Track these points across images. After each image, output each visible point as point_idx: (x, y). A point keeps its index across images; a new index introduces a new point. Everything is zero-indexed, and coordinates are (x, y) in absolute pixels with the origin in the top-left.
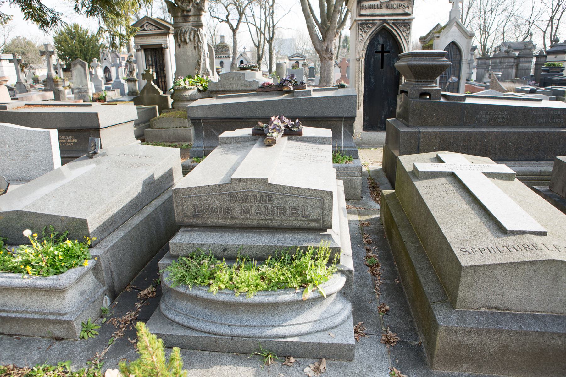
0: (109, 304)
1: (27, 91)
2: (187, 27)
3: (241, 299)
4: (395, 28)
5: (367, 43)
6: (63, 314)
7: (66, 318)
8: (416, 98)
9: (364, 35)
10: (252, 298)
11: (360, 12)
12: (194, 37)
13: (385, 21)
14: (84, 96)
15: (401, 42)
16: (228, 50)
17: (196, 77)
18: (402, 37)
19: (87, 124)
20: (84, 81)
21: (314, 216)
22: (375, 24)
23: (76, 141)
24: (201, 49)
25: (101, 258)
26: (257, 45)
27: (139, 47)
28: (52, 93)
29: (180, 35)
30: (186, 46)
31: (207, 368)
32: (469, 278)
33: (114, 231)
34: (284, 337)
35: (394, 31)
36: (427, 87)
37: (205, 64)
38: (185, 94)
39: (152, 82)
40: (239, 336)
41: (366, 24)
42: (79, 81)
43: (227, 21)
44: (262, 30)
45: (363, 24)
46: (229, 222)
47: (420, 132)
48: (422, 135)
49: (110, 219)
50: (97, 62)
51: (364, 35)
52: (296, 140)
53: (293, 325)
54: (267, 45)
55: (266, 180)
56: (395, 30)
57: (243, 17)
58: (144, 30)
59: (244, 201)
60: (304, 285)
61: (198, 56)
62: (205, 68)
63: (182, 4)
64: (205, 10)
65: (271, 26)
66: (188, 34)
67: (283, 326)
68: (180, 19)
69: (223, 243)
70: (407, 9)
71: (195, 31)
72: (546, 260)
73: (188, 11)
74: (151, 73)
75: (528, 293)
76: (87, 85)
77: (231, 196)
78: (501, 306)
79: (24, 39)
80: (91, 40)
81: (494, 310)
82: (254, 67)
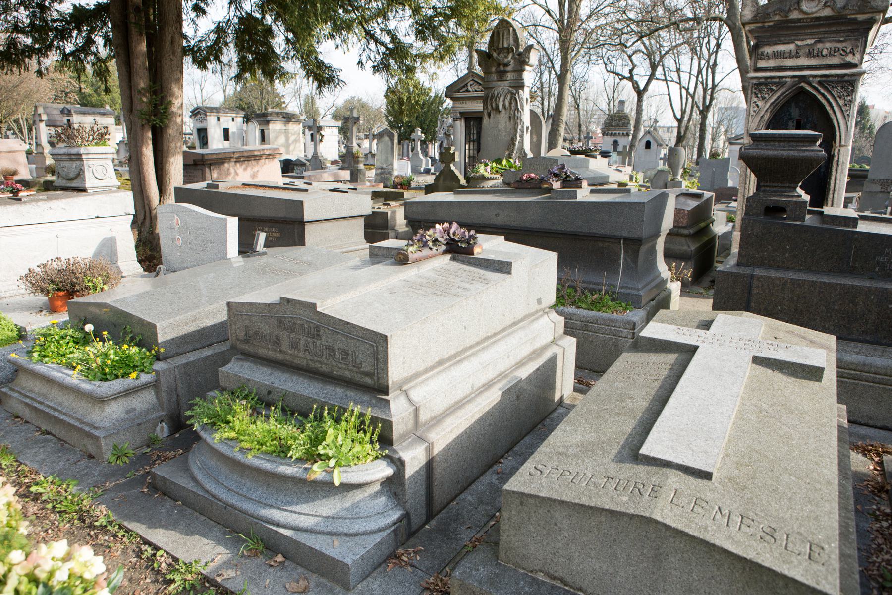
0: (166, 435)
1: (322, 168)
2: (502, 87)
3: (240, 457)
4: (822, 91)
6: (96, 428)
7: (97, 433)
8: (757, 215)
10: (250, 459)
11: (756, 64)
12: (510, 103)
13: (803, 79)
14: (387, 179)
15: (833, 116)
16: (629, 123)
17: (504, 162)
18: (836, 108)
19: (291, 215)
20: (390, 159)
21: (366, 368)
23: (278, 235)
24: (519, 121)
25: (161, 374)
26: (679, 117)
28: (349, 172)
29: (491, 99)
31: (187, 535)
32: (513, 512)
33: (204, 347)
34: (278, 525)
35: (819, 97)
36: (781, 196)
37: (522, 142)
39: (452, 165)
40: (232, 506)
41: (766, 85)
42: (384, 157)
43: (631, 78)
44: (691, 91)
46: (279, 357)
47: (752, 276)
48: (755, 282)
49: (198, 331)
50: (419, 133)
51: (759, 103)
52: (463, 262)
53: (296, 513)
54: (696, 116)
56: (823, 95)
57: (659, 70)
58: (468, 91)
59: (293, 331)
60: (312, 457)
61: (512, 131)
62: (522, 149)
64: (531, 63)
65: (710, 86)
66: (502, 98)
67: (283, 510)
68: (494, 77)
70: (850, 55)
71: (512, 93)
72: (638, 516)
73: (506, 65)
74: (452, 152)
75: (611, 570)
77: (280, 321)
78: (569, 579)
79: (359, 100)
80: (432, 103)
81: (558, 584)
82: (592, 151)
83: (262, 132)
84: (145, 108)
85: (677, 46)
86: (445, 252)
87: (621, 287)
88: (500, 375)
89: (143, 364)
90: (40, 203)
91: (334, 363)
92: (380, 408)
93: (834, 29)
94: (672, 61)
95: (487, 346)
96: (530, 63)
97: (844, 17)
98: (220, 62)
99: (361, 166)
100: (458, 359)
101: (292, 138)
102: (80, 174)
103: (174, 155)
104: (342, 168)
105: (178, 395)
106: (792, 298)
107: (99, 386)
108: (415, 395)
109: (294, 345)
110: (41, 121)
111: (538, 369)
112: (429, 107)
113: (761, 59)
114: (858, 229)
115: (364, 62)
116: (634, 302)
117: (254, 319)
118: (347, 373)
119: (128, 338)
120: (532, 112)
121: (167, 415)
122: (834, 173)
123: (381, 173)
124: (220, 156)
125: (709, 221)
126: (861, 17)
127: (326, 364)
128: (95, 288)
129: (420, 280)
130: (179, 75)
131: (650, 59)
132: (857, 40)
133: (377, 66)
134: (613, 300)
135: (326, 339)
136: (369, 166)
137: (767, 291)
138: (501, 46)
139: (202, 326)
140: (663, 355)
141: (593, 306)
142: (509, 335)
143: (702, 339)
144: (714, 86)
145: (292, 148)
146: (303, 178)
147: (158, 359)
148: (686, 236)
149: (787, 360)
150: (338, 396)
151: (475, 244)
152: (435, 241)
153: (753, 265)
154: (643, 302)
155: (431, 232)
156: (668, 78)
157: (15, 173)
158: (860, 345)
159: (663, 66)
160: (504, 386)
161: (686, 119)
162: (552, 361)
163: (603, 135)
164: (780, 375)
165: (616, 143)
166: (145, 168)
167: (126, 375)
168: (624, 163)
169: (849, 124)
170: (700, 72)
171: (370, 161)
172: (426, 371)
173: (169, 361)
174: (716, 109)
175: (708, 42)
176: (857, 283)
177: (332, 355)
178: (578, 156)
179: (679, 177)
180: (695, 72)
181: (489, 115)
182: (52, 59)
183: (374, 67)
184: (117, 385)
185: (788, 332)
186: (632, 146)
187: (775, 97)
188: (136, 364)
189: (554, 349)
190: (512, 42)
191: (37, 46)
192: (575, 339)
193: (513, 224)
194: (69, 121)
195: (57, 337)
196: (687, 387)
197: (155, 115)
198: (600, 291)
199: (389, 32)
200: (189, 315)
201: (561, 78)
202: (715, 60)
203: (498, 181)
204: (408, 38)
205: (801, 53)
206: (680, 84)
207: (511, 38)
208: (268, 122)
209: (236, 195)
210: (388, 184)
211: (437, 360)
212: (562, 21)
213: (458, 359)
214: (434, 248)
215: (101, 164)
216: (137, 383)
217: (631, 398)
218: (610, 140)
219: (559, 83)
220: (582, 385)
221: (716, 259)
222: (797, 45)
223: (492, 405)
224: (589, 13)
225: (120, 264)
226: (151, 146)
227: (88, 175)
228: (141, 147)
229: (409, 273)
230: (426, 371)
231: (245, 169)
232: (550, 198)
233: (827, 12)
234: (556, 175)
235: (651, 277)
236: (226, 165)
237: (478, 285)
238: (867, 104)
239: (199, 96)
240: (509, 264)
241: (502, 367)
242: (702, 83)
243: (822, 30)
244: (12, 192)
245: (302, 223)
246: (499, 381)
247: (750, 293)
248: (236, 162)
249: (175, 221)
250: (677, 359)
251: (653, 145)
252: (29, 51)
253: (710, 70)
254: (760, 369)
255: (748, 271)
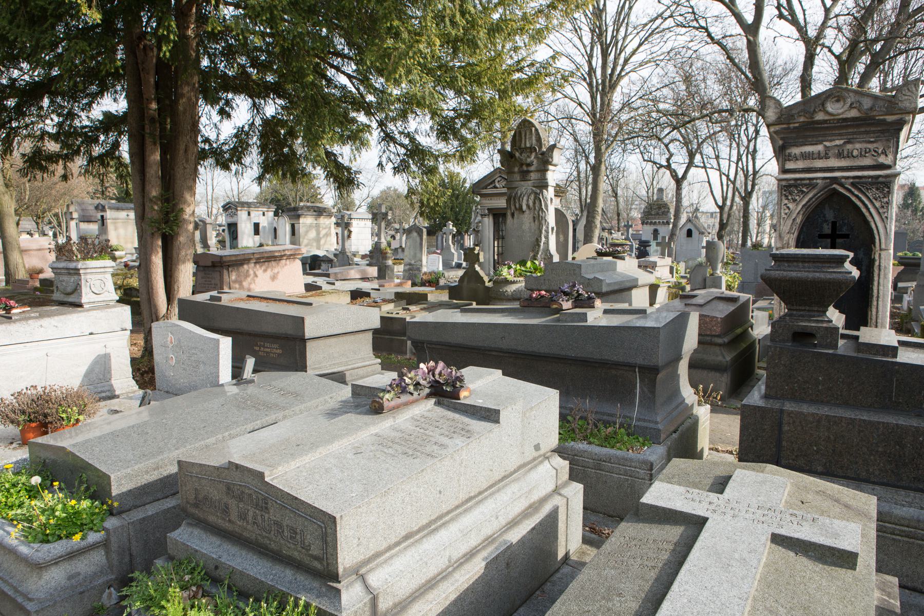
1: (350, 264)
2: (525, 187)
4: (856, 193)
5: (799, 220)
6: (30, 600)
9: (791, 206)
11: (783, 165)
12: (534, 203)
13: (835, 180)
14: (415, 276)
15: (870, 219)
16: (668, 212)
17: (529, 264)
19: (289, 330)
20: (418, 255)
21: (315, 551)
22: (814, 186)
23: (279, 351)
24: (543, 222)
25: (112, 533)
27: (487, 211)
30: (522, 216)
33: (166, 497)
35: (854, 199)
36: (810, 321)
37: (547, 243)
38: (505, 289)
39: (476, 266)
41: (796, 186)
43: (668, 167)
44: (732, 177)
45: (790, 186)
47: (782, 411)
48: (786, 419)
49: (161, 480)
50: (451, 227)
51: (791, 206)
55: (261, 475)
56: (857, 196)
57: (698, 157)
58: (495, 187)
59: (241, 500)
61: (537, 232)
62: (547, 250)
63: (521, 154)
65: (751, 172)
66: (525, 198)
68: (517, 177)
69: (214, 556)
70: (883, 156)
71: (536, 193)
73: (529, 165)
74: (476, 252)
76: (421, 261)
77: (229, 488)
79: (395, 190)
80: (467, 194)
83: (293, 226)
84: (155, 215)
85: (715, 133)
86: (429, 396)
87: (638, 420)
88: (486, 539)
89: (92, 521)
90: (30, 322)
91: (282, 542)
92: (330, 599)
93: (863, 130)
94: (711, 148)
95: (471, 508)
96: (554, 162)
97: (873, 118)
98: (242, 164)
99: (390, 262)
100: (433, 527)
101: (323, 232)
102: (77, 289)
103: (184, 262)
104: (370, 265)
105: (131, 555)
106: (829, 438)
107: (37, 551)
108: (374, 580)
109: (243, 516)
110: (72, 219)
111: (533, 529)
112: (464, 198)
113: (789, 160)
114: (899, 360)
115: (384, 164)
116: (652, 437)
117: (204, 482)
118: (296, 553)
119: (82, 488)
120: (557, 210)
121: (116, 579)
122: (876, 278)
123: (410, 269)
124: (239, 258)
125: (746, 326)
126: (890, 118)
127: (275, 542)
128: (69, 419)
129: (394, 434)
130: (191, 182)
131: (688, 148)
132: (888, 140)
133: (398, 167)
134: (628, 435)
135: (274, 514)
136: (397, 261)
137: (799, 428)
138: (523, 146)
139: (165, 474)
140: (668, 527)
141: (607, 441)
142: (499, 490)
143: (712, 507)
144: (755, 173)
145: (322, 242)
146: (328, 276)
147: (112, 514)
148: (720, 345)
149: (814, 540)
150: (287, 579)
151: (462, 387)
152: (417, 384)
153: (782, 397)
154: (663, 436)
155: (412, 374)
156: (708, 166)
157: (41, 271)
158: (912, 494)
159: (701, 154)
160: (490, 555)
161: (728, 203)
162: (553, 517)
163: (643, 224)
164: (804, 560)
165: (656, 232)
166: (154, 276)
167: (69, 536)
168: (663, 254)
169: (888, 227)
170: (739, 158)
171: (400, 256)
172: (389, 548)
173: (124, 516)
174: (760, 194)
175: (747, 129)
176: (902, 421)
177: (280, 533)
178: (605, 258)
179: (718, 272)
180: (734, 158)
181: (513, 215)
182: (80, 161)
183: (394, 168)
184: (58, 548)
185: (818, 493)
186: (672, 235)
187: (806, 199)
188: (84, 521)
189: (557, 501)
190: (534, 142)
191: (65, 152)
192: (582, 486)
193: (520, 348)
194: (102, 217)
195: (7, 485)
196: (687, 583)
197: (166, 223)
198: (615, 423)
199: (408, 135)
200: (151, 462)
201: (596, 169)
202: (755, 146)
203: (520, 285)
204: (428, 140)
205: (830, 154)
206: (719, 170)
207: (534, 138)
208: (298, 217)
209: (238, 308)
210: (418, 280)
211: (403, 533)
212: (594, 115)
213: (433, 527)
214: (416, 393)
215: (98, 280)
216: (84, 543)
217: (620, 595)
218: (649, 229)
219: (593, 174)
220: (594, 536)
221: (757, 364)
222: (825, 146)
223: (474, 579)
224: (621, 106)
225: (113, 382)
226: (160, 254)
227: (85, 290)
228: (151, 255)
229: (383, 425)
230: (389, 548)
231: (265, 271)
232: (558, 320)
233: (854, 113)
234: (566, 294)
235: (673, 406)
236: (246, 266)
237: (459, 441)
238: (917, 185)
239: (235, 188)
240: (497, 412)
241: (487, 531)
242: (743, 169)
243: (850, 130)
244: (4, 309)
245: (301, 341)
246: (484, 548)
247: (780, 431)
248: (255, 263)
249: (169, 339)
250: (681, 535)
251: (695, 233)
252: (53, 158)
253: (750, 156)
254: (781, 551)
255: (776, 405)
